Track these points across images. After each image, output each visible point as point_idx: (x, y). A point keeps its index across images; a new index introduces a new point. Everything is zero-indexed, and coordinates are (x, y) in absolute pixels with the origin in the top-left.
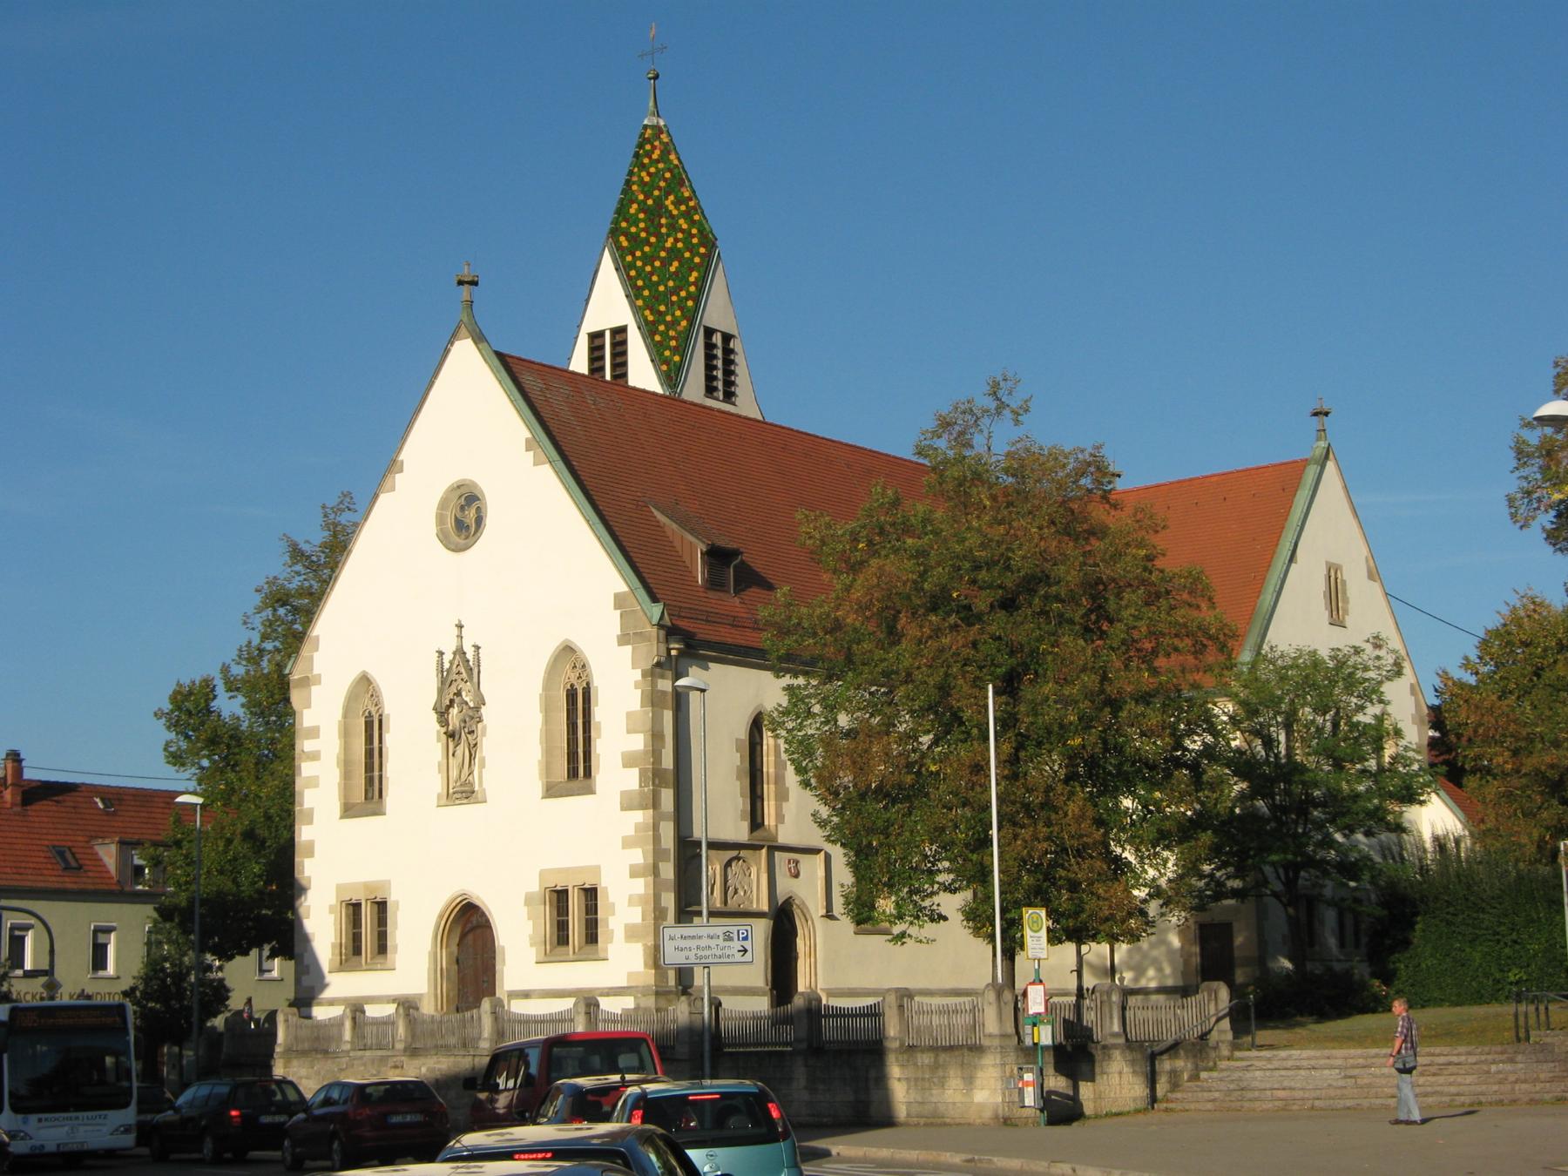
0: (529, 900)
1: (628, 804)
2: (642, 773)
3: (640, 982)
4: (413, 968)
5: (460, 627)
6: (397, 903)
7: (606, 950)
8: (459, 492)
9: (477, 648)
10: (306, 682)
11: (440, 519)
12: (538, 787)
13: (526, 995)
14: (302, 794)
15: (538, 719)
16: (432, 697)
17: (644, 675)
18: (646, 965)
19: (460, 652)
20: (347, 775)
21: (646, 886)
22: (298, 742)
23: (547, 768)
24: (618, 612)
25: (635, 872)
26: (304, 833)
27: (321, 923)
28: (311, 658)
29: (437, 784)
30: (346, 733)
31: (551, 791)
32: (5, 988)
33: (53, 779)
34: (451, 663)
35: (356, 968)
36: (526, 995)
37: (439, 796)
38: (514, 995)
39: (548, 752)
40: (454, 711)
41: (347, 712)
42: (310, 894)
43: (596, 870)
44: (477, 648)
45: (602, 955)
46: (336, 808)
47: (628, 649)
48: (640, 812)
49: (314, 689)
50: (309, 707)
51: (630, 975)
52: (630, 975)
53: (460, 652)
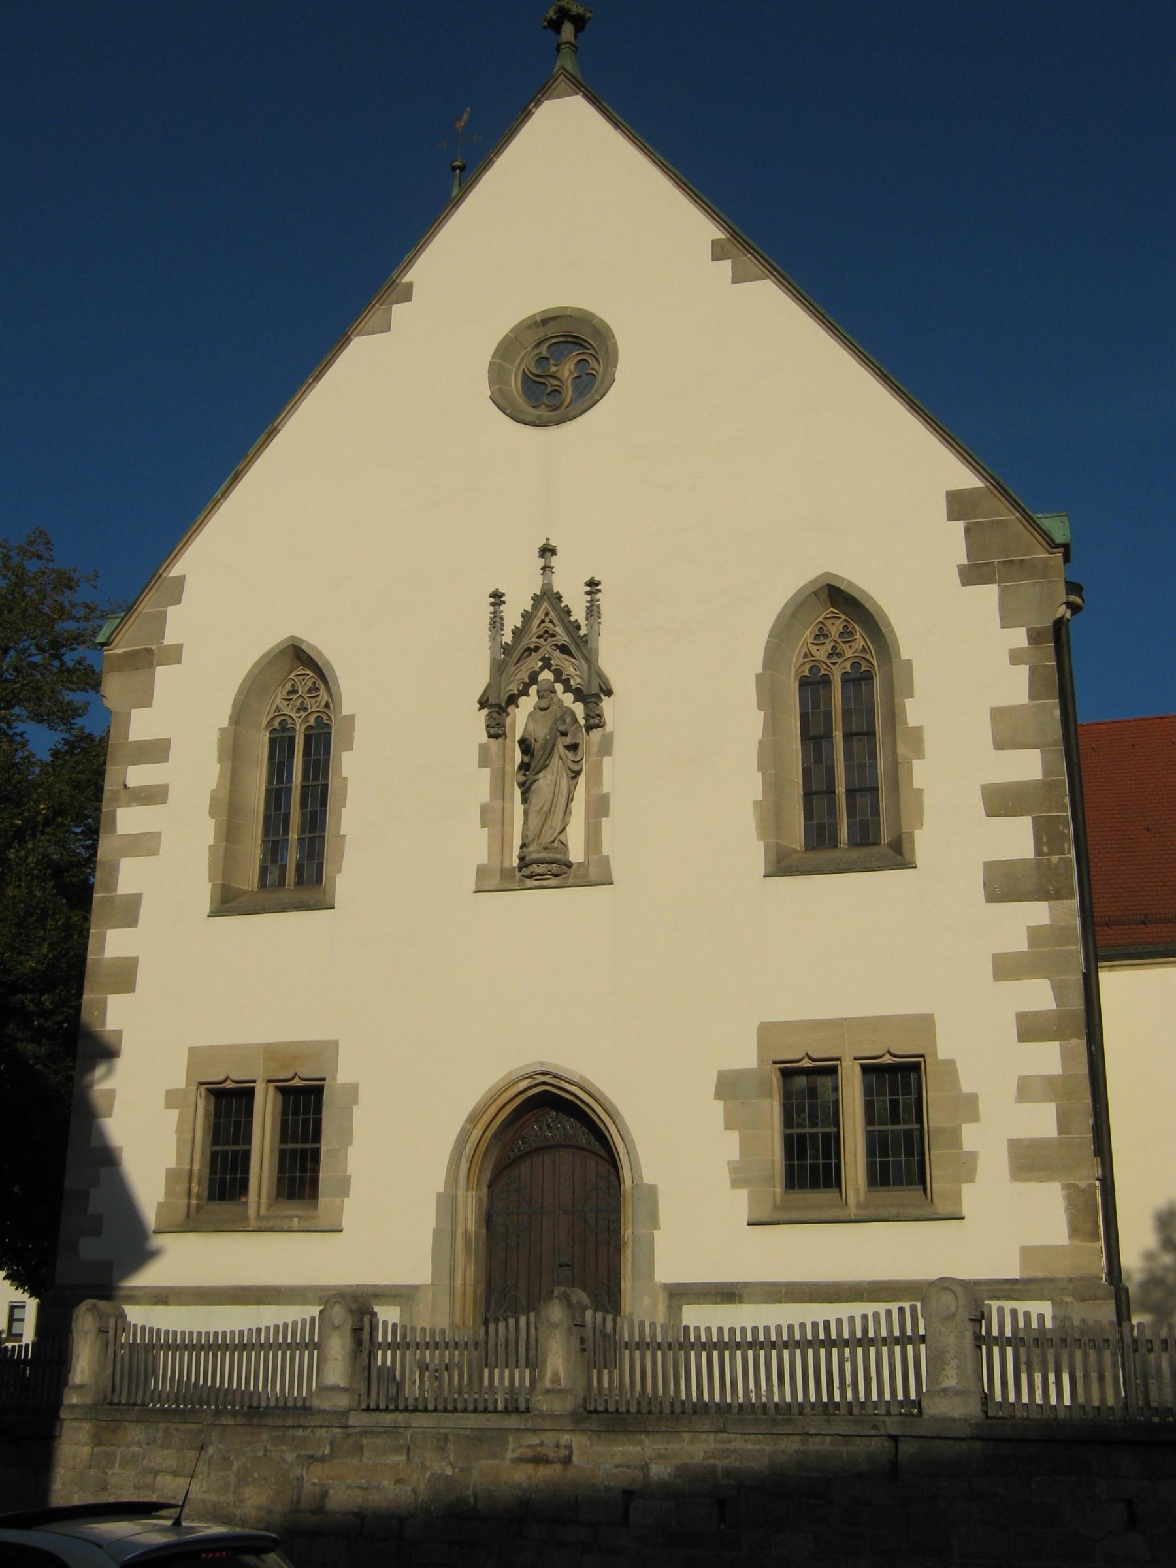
0: (729, 1086)
1: (1003, 884)
2: (111, 886)
3: (1062, 1269)
4: (393, 1220)
5: (547, 551)
6: (353, 1091)
7: (957, 1198)
8: (541, 333)
9: (593, 585)
10: (145, 660)
11: (497, 373)
12: (756, 855)
13: (728, 1294)
14: (114, 870)
15: (755, 721)
16: (481, 678)
17: (1035, 637)
18: (1075, 1231)
19: (548, 597)
20: (230, 832)
21: (1066, 1057)
22: (110, 769)
23: (770, 817)
24: (960, 525)
25: (1031, 1029)
26: (113, 943)
27: (144, 1127)
28: (162, 618)
29: (476, 847)
30: (233, 749)
31: (228, 902)
32: (1167, 1259)
33: (799, 731)
34: (527, 616)
35: (238, 1225)
36: (728, 1294)
37: (482, 872)
38: (680, 1294)
39: (774, 785)
40: (527, 704)
41: (773, 657)
42: (121, 1063)
43: (925, 1023)
44: (593, 584)
45: (941, 1207)
46: (202, 892)
47: (990, 592)
48: (1044, 905)
49: (163, 673)
50: (148, 703)
51: (1027, 1253)
52: (1027, 1253)
53: (548, 597)
